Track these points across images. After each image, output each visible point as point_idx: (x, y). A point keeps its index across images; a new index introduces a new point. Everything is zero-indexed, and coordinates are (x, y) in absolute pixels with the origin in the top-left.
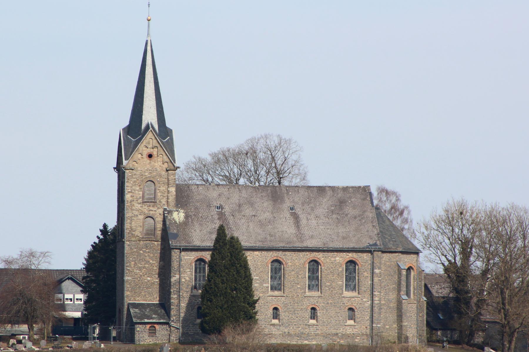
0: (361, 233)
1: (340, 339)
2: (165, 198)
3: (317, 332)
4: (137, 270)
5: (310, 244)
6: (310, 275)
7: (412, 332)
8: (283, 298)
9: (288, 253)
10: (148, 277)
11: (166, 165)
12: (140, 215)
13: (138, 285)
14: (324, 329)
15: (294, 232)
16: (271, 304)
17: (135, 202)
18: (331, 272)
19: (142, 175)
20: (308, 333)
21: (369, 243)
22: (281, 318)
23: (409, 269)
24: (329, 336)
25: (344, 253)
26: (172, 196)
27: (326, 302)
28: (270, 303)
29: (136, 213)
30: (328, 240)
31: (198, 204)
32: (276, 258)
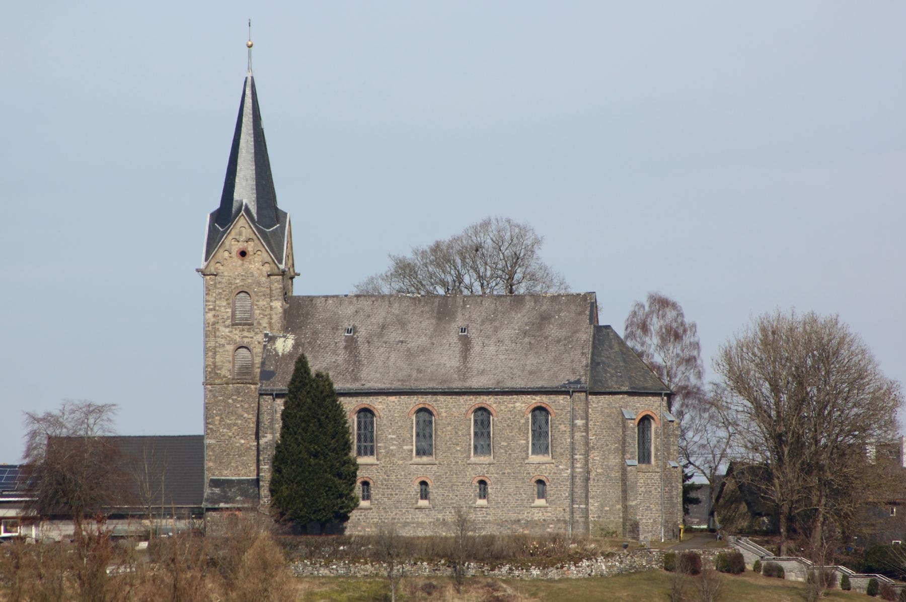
0: (561, 365)
2: (266, 318)
3: (488, 519)
4: (224, 428)
5: (475, 383)
6: (477, 430)
7: (652, 516)
8: (434, 466)
10: (242, 438)
11: (267, 268)
12: (229, 344)
13: (225, 451)
14: (498, 513)
15: (457, 364)
16: (415, 477)
18: (508, 426)
19: (231, 283)
21: (568, 380)
22: (432, 497)
23: (645, 421)
24: (506, 523)
25: (529, 396)
26: (276, 314)
27: (501, 472)
28: (414, 474)
29: (223, 341)
30: (505, 376)
31: (319, 327)
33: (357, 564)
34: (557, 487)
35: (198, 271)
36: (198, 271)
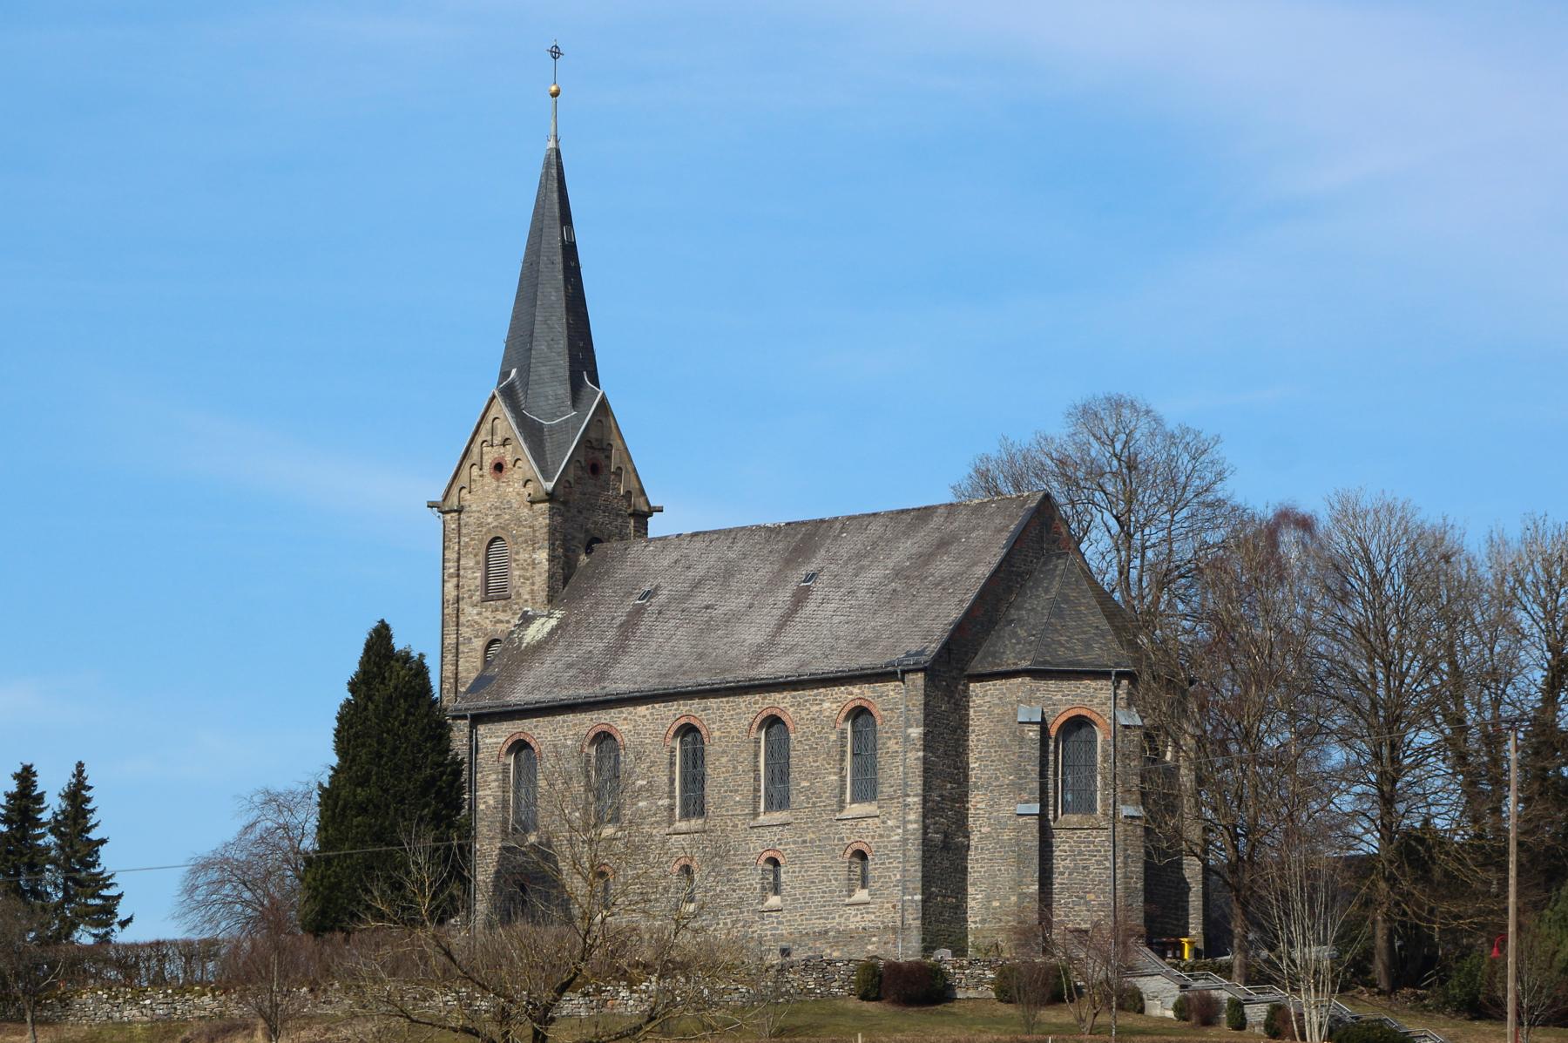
1: (831, 947)
9: (713, 703)
17: (466, 603)
19: (480, 525)
20: (760, 936)
24: (806, 938)
25: (843, 688)
26: (540, 575)
27: (800, 840)
32: (687, 721)
33: (187, 996)
34: (883, 864)
35: (431, 505)
36: (431, 505)
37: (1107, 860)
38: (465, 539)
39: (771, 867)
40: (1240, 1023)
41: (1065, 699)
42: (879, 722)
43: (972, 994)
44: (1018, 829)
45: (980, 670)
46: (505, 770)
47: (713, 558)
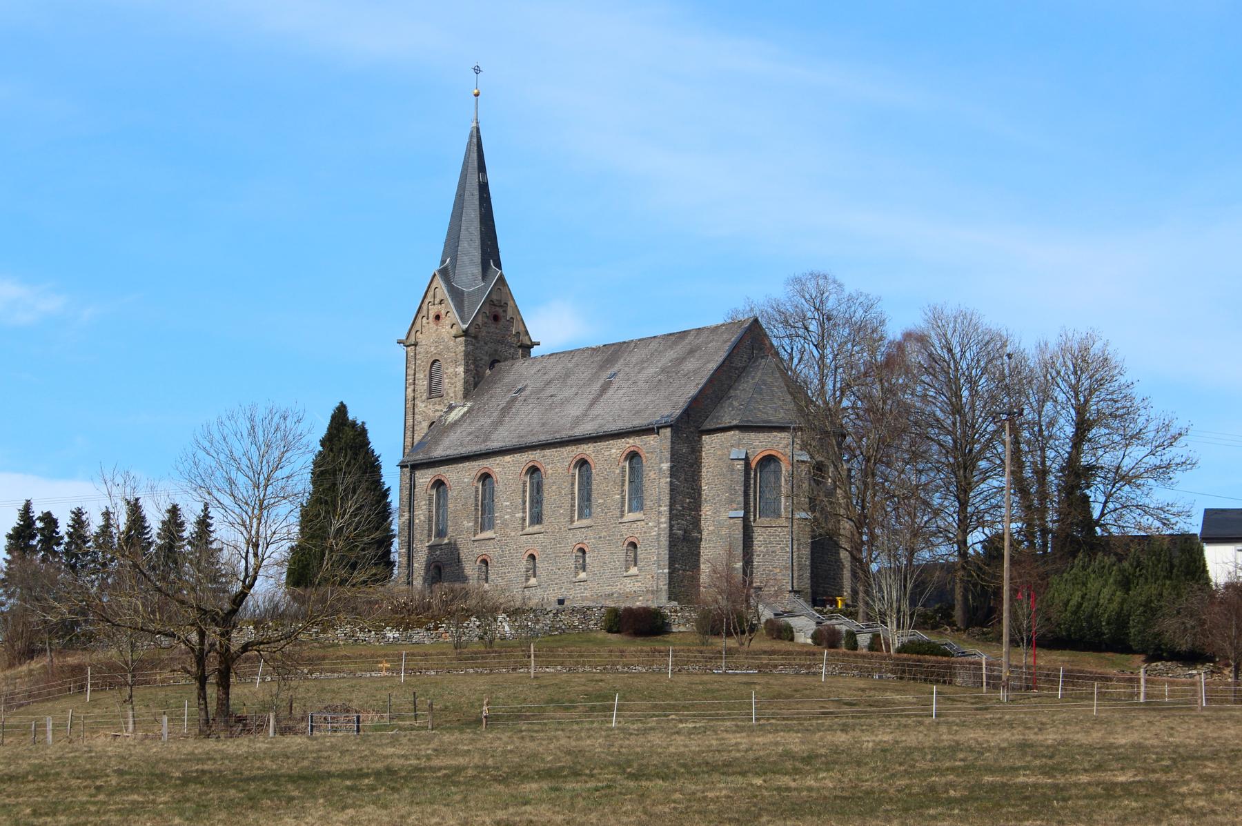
9: (548, 452)
35: (399, 342)
36: (399, 342)
37: (787, 546)
38: (418, 362)
39: (581, 554)
40: (854, 645)
41: (760, 444)
42: (644, 461)
43: (682, 629)
44: (730, 527)
45: (709, 427)
46: (430, 499)
47: (559, 368)
